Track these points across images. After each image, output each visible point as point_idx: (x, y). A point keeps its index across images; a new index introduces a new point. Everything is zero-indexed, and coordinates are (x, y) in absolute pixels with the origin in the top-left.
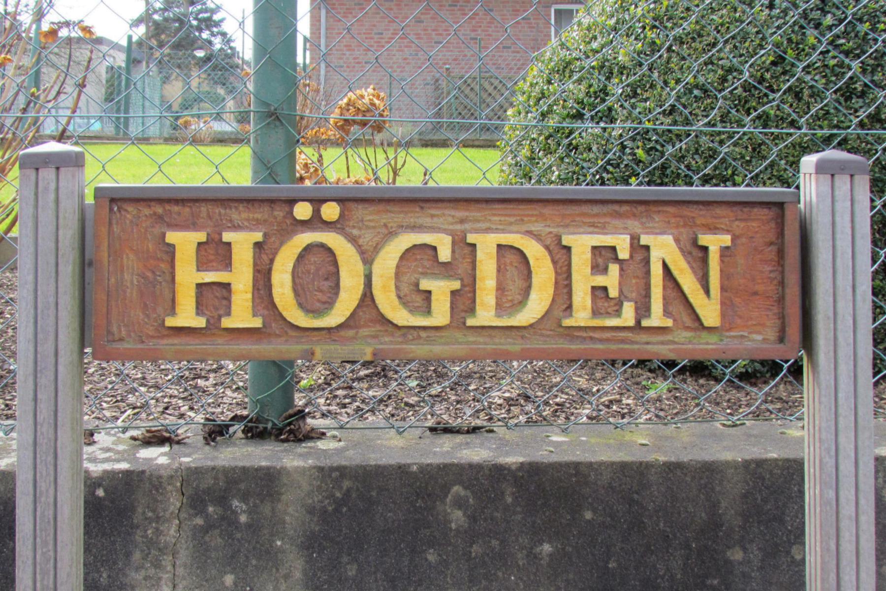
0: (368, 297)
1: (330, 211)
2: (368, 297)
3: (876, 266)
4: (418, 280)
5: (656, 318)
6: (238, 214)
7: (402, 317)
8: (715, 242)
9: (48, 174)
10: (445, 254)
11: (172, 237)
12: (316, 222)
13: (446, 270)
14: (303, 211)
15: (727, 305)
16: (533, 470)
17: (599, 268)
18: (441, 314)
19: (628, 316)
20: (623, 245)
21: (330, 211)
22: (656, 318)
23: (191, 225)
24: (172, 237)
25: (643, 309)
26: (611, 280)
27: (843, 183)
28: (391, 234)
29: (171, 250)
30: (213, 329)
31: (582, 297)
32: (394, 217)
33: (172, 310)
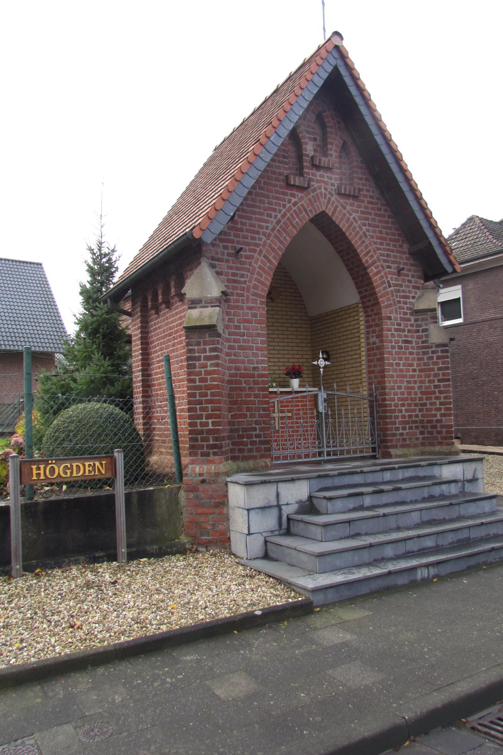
0: (59, 473)
1: (54, 462)
2: (59, 473)
3: (29, 502)
4: (439, 303)
5: (97, 473)
6: (41, 463)
7: (64, 476)
8: (104, 462)
9: (15, 459)
10: (69, 467)
11: (32, 467)
12: (52, 463)
13: (69, 469)
14: (50, 462)
15: (106, 471)
16: (75, 499)
17: (89, 467)
18: (69, 475)
19: (93, 473)
20: (92, 463)
21: (54, 462)
22: (97, 473)
23: (34, 465)
24: (32, 467)
25: (95, 472)
26: (91, 468)
27: (120, 454)
28: (61, 464)
29: (32, 469)
30: (38, 479)
31: (87, 471)
32: (62, 462)
33: (32, 477)
